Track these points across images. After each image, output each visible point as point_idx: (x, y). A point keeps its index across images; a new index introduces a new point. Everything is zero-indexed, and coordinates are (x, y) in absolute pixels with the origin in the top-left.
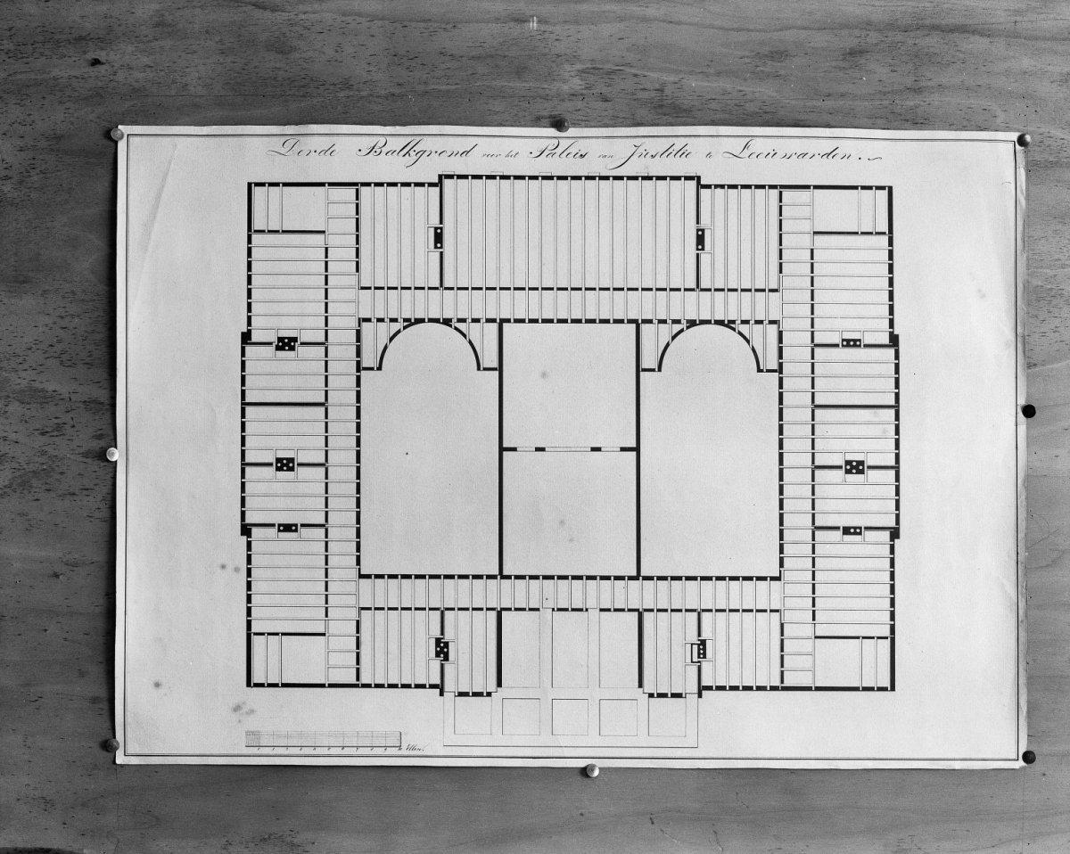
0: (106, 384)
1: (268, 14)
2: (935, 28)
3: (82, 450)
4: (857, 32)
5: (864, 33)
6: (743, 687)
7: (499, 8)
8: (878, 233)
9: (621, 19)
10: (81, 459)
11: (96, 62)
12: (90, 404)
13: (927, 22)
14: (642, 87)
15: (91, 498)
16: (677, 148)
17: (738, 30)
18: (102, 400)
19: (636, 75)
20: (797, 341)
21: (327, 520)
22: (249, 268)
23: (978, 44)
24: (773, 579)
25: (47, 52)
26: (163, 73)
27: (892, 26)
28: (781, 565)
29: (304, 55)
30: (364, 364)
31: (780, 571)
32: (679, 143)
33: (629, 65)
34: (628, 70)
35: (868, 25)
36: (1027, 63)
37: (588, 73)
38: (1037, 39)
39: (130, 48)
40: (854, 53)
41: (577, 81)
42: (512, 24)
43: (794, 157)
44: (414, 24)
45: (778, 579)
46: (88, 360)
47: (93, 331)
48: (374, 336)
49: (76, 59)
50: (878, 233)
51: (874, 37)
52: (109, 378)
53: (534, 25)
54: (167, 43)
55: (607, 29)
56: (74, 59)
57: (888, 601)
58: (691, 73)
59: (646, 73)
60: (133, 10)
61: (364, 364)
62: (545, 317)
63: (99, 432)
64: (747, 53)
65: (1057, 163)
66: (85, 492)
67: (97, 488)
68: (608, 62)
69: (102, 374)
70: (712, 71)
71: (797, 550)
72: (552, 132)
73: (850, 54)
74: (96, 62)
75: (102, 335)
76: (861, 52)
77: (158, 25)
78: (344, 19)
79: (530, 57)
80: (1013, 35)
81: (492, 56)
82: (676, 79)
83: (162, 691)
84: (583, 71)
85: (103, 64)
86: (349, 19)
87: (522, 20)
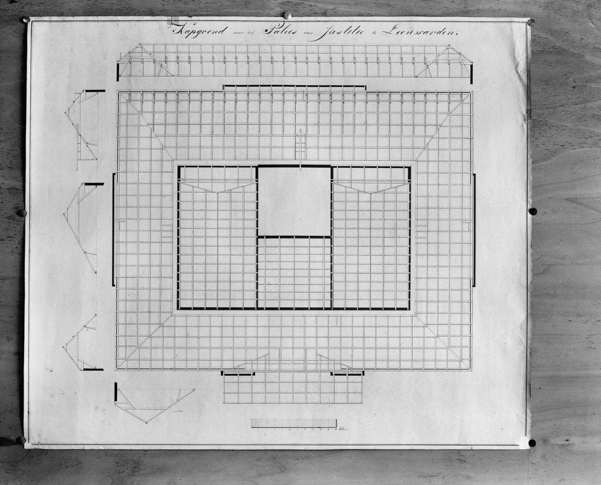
0: (20, 179)
3: (7, 216)
6: (206, 308)
10: (7, 220)
12: (11, 190)
14: (314, 12)
15: (12, 242)
16: (353, 29)
18: (17, 187)
19: (311, 6)
26: (49, 7)
32: (355, 25)
37: (284, 5)
43: (422, 33)
46: (10, 166)
47: (12, 150)
52: (21, 175)
63: (16, 206)
65: (543, 51)
66: (9, 239)
67: (16, 236)
69: (18, 173)
72: (281, 19)
75: (18, 151)
82: (334, 8)
83: (52, 373)
85: (16, 2)
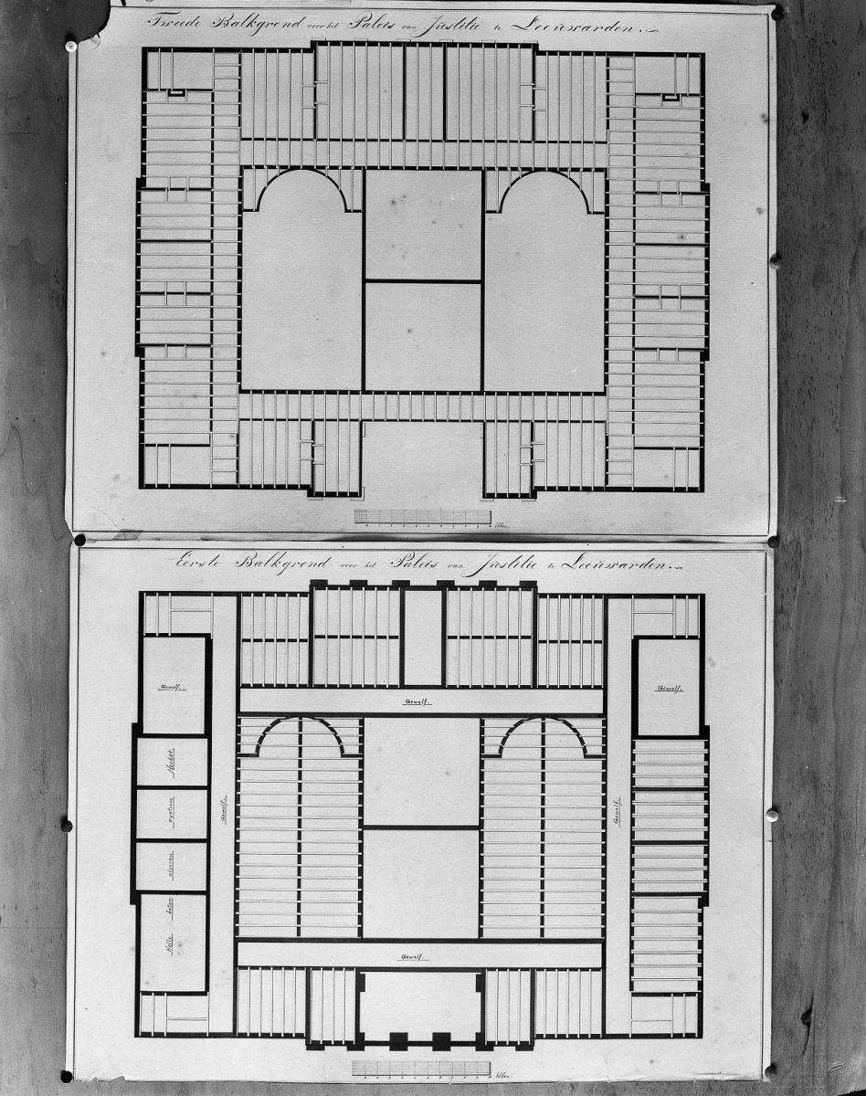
1: (847, 267)
2: (837, 852)
4: (833, 784)
5: (833, 789)
7: (855, 469)
8: (607, 476)
9: (844, 576)
11: (805, 117)
13: (842, 845)
17: (835, 680)
19: (795, 589)
20: (621, 188)
21: (212, 290)
22: (606, 357)
23: (823, 885)
24: (597, 394)
25: (814, 75)
27: (839, 814)
28: (606, 381)
29: (812, 299)
30: (245, 207)
31: (605, 388)
33: (804, 583)
34: (799, 583)
35: (839, 793)
36: (807, 932)
38: (828, 941)
39: (818, 147)
40: (814, 780)
41: (790, 538)
42: (839, 480)
44: (839, 395)
45: (603, 394)
48: (254, 181)
49: (808, 100)
50: (607, 476)
51: (829, 798)
53: (839, 500)
54: (822, 179)
55: (835, 564)
56: (808, 97)
57: (703, 224)
58: (797, 639)
59: (796, 598)
60: (851, 150)
61: (245, 207)
62: (546, 835)
64: (814, 686)
68: (807, 565)
70: (799, 656)
71: (619, 368)
73: (814, 777)
74: (805, 117)
76: (816, 787)
77: (838, 171)
78: (844, 332)
79: (811, 497)
80: (831, 922)
81: (811, 463)
84: (799, 543)
86: (844, 337)
87: (843, 490)
